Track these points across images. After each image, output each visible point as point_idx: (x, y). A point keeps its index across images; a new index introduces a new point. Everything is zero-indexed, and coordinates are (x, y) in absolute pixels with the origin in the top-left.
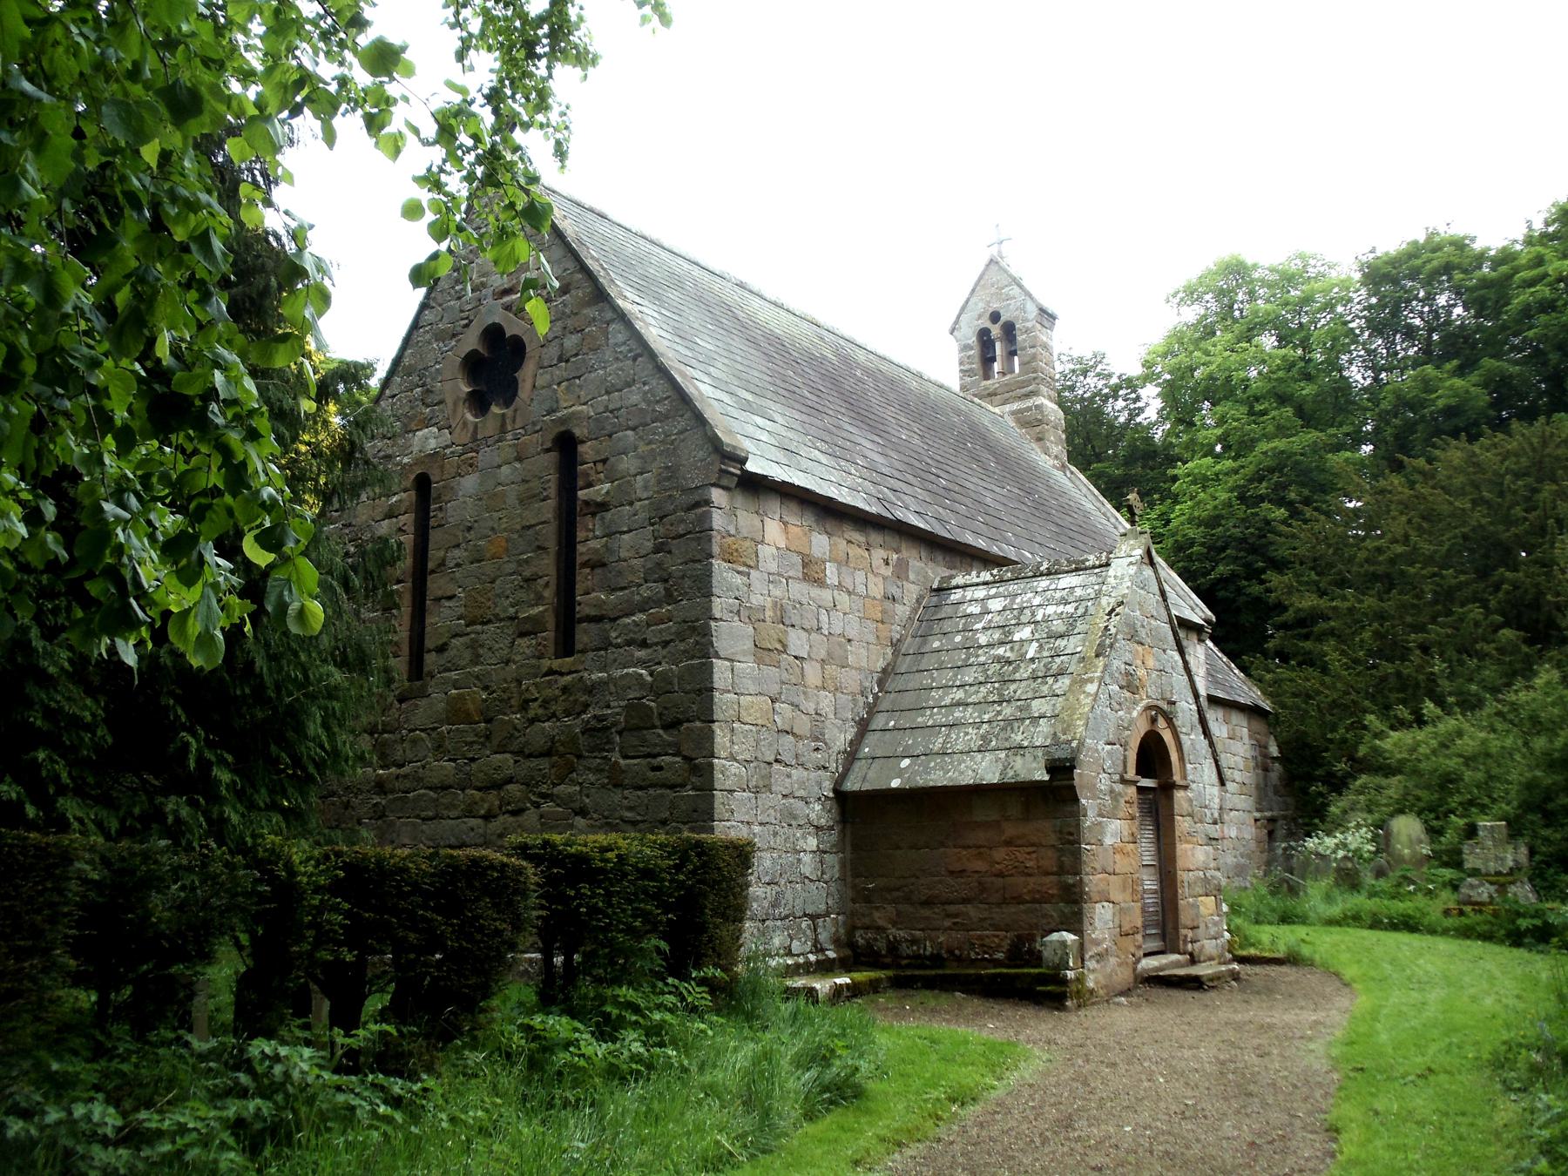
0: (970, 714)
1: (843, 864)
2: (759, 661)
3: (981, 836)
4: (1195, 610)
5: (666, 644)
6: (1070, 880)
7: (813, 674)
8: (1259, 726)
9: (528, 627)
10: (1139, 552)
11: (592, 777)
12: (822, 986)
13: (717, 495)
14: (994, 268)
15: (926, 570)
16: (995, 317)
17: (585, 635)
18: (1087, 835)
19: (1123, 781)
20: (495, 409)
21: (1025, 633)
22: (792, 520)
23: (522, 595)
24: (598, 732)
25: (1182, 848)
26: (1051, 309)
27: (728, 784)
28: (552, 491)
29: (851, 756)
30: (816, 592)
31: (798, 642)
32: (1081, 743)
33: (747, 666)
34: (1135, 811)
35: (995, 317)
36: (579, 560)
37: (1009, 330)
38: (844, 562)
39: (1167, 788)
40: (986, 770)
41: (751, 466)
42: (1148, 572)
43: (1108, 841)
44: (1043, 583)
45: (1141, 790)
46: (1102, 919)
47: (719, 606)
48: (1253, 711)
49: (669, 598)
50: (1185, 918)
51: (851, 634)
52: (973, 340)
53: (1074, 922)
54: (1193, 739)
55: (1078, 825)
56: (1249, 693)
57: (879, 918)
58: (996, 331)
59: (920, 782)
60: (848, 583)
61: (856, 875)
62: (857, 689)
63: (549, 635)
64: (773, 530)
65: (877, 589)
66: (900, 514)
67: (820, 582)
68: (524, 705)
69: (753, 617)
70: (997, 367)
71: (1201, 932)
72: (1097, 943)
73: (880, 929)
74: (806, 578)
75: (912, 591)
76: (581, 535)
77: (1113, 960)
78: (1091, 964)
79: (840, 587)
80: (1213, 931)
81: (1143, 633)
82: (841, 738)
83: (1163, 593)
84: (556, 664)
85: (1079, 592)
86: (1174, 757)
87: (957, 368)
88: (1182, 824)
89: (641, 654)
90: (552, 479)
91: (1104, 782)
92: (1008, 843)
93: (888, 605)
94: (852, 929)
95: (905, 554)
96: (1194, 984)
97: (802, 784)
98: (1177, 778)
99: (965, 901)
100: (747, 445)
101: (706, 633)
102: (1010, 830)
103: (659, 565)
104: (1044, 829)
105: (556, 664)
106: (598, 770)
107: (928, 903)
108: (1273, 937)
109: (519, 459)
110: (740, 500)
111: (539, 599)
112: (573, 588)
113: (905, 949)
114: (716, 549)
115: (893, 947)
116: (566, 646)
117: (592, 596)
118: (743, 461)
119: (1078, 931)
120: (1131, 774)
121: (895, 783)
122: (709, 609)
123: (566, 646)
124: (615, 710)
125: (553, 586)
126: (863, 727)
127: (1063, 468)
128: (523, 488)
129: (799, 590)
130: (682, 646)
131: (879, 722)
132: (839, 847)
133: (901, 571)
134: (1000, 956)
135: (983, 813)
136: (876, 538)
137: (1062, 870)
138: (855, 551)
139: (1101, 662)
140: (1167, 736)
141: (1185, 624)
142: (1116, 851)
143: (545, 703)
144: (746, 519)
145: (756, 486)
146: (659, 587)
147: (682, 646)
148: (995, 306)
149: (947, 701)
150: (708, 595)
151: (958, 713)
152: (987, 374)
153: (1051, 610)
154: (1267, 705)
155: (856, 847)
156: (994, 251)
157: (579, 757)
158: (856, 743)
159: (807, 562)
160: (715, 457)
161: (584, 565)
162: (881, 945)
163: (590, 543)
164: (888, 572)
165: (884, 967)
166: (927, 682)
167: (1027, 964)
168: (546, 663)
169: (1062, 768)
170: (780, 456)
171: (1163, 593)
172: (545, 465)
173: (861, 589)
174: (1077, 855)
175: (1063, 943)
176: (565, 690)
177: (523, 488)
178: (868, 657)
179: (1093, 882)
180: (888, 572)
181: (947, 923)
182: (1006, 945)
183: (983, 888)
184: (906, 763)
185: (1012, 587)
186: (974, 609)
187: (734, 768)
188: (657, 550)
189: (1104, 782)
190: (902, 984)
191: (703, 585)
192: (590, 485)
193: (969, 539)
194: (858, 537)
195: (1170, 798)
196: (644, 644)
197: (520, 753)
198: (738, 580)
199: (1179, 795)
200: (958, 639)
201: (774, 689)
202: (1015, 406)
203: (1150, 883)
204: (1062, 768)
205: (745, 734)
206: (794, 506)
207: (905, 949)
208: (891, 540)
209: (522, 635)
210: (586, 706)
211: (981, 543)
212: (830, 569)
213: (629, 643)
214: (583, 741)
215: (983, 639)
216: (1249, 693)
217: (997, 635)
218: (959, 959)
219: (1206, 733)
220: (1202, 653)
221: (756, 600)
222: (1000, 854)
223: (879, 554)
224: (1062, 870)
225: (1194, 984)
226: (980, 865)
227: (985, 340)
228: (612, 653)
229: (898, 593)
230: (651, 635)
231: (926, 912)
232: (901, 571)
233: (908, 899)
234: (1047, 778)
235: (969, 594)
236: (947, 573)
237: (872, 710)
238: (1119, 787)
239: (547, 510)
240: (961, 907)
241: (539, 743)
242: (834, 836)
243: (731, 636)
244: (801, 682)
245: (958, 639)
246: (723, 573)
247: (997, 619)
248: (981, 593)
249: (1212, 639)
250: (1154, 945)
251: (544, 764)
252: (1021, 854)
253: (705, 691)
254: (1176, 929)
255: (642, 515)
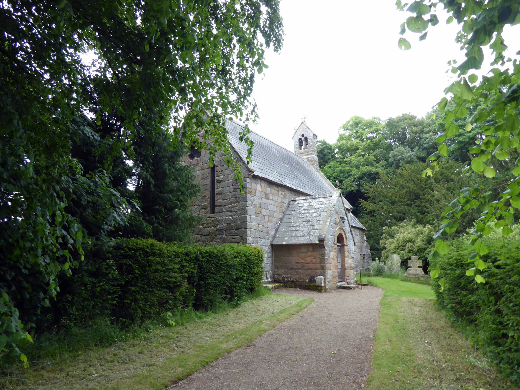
0: (300, 228)
1: (272, 261)
2: (256, 216)
3: (303, 255)
4: (348, 205)
5: (236, 212)
6: (323, 265)
7: (267, 219)
8: (361, 232)
9: (204, 207)
10: (338, 194)
11: (218, 240)
12: (270, 286)
13: (248, 180)
14: (303, 124)
15: (290, 196)
16: (303, 136)
17: (217, 209)
18: (327, 255)
19: (334, 244)
20: (195, 158)
21: (313, 211)
22: (263, 185)
23: (202, 200)
24: (221, 231)
25: (346, 259)
26: (316, 134)
27: (250, 242)
28: (209, 177)
29: (274, 237)
30: (268, 201)
31: (264, 212)
32: (326, 235)
33: (254, 217)
34: (336, 250)
35: (303, 136)
36: (216, 193)
37: (306, 139)
38: (273, 194)
39: (343, 246)
40: (302, 240)
41: (255, 173)
42: (340, 198)
43: (331, 257)
44: (317, 200)
45: (338, 246)
46: (329, 273)
47: (248, 204)
48: (361, 229)
49: (237, 202)
50: (347, 274)
51: (275, 210)
52: (297, 141)
53: (324, 274)
54: (349, 235)
55: (325, 253)
56: (360, 225)
57: (280, 272)
58: (303, 139)
59: (290, 243)
60: (274, 199)
61: (275, 263)
62: (275, 222)
63: (208, 209)
64: (259, 187)
65: (280, 201)
66: (285, 184)
67: (268, 199)
68: (203, 224)
69: (255, 206)
70: (303, 147)
71: (350, 278)
72: (328, 279)
73: (280, 275)
74: (265, 198)
75: (287, 201)
76: (216, 187)
77: (331, 283)
78: (327, 283)
79: (272, 200)
80: (352, 278)
81: (339, 212)
82: (272, 232)
83: (343, 203)
84: (211, 215)
85: (325, 202)
86: (345, 239)
87: (294, 147)
88: (346, 254)
89: (231, 214)
90: (209, 174)
91: (330, 244)
92: (309, 256)
93: (282, 204)
94: (274, 275)
95: (286, 192)
96: (350, 288)
97: (264, 243)
98: (345, 244)
99: (299, 269)
100: (254, 168)
101: (245, 210)
102: (309, 254)
103: (234, 194)
104: (317, 254)
105: (211, 215)
106: (220, 239)
107: (291, 269)
108: (365, 280)
109: (201, 170)
110: (253, 181)
111: (206, 201)
112: (214, 199)
113: (286, 279)
114: (247, 192)
115: (283, 278)
116: (213, 211)
117: (219, 201)
118: (253, 172)
119: (324, 276)
120: (336, 242)
121: (284, 243)
122: (246, 204)
123: (213, 211)
124: (224, 226)
125: (210, 198)
126: (277, 230)
127: (318, 171)
128: (202, 176)
129: (264, 200)
130: (240, 212)
131: (280, 229)
132: (272, 257)
133: (285, 196)
134: (307, 281)
135: (304, 250)
136: (280, 189)
137: (321, 263)
138: (276, 192)
139: (330, 218)
140: (343, 235)
141: (347, 209)
142: (332, 259)
143: (208, 224)
144: (254, 185)
145: (255, 177)
146: (235, 199)
147: (240, 212)
148: (303, 133)
149: (295, 225)
150: (246, 201)
151: (298, 228)
152: (301, 149)
153: (318, 206)
154: (364, 228)
155: (275, 256)
156: (303, 120)
157: (216, 236)
158: (275, 234)
159: (266, 194)
160: (248, 172)
161: (217, 194)
162: (281, 278)
163: (217, 191)
164: (282, 196)
165: (281, 283)
166: (291, 221)
167: (313, 283)
168: (208, 215)
169: (321, 241)
170: (260, 171)
171: (343, 203)
172: (208, 171)
173: (277, 200)
174: (324, 259)
175: (321, 278)
176: (212, 221)
177: (202, 176)
178: (278, 215)
179: (328, 265)
180: (282, 196)
181: (295, 273)
182: (308, 278)
183: (303, 266)
184: (286, 238)
185: (310, 201)
186: (301, 205)
187: (251, 239)
188: (234, 191)
189: (330, 244)
190: (285, 286)
191: (245, 199)
192: (218, 176)
193: (299, 189)
194: (276, 188)
195: (344, 248)
196: (231, 212)
197: (202, 235)
198: (252, 198)
199: (345, 247)
200: (298, 212)
201: (259, 222)
202: (307, 156)
203: (340, 267)
204: (321, 241)
205: (253, 231)
206: (263, 182)
207: (286, 279)
208: (283, 189)
209: (202, 209)
210: (217, 225)
211: (302, 190)
212: (270, 196)
213: (227, 211)
214: (217, 232)
215: (303, 212)
216: (360, 225)
217: (306, 211)
218: (298, 281)
219: (352, 234)
220: (350, 215)
221: (255, 202)
222: (307, 259)
223: (280, 192)
224: (321, 263)
225: (350, 288)
226: (303, 261)
227: (300, 141)
228: (223, 213)
229: (284, 201)
230: (232, 210)
231: (291, 271)
232: (285, 196)
233: (287, 268)
234: (318, 242)
235: (300, 202)
236: (294, 197)
237: (279, 227)
238: (333, 245)
239: (208, 181)
240: (298, 270)
241: (207, 233)
242: (270, 254)
243: (250, 210)
244: (264, 220)
245: (298, 212)
246: (249, 197)
247: (307, 208)
248: (302, 202)
249: (352, 212)
250: (340, 280)
251: (208, 237)
252: (312, 259)
253: (245, 222)
254: (345, 276)
255: (230, 184)
